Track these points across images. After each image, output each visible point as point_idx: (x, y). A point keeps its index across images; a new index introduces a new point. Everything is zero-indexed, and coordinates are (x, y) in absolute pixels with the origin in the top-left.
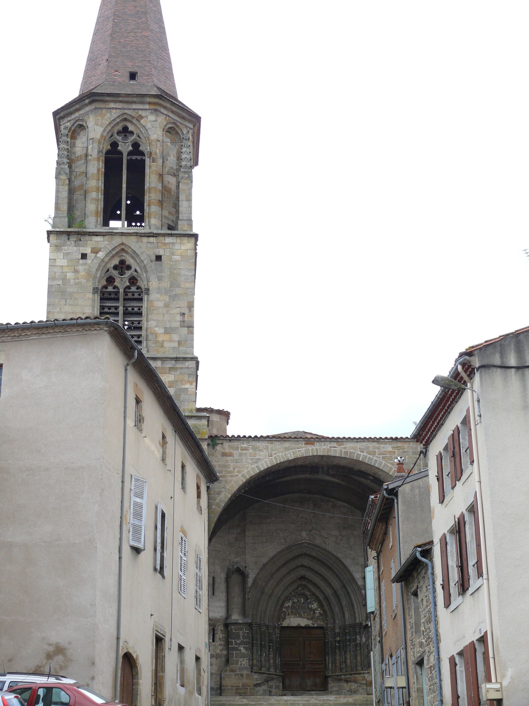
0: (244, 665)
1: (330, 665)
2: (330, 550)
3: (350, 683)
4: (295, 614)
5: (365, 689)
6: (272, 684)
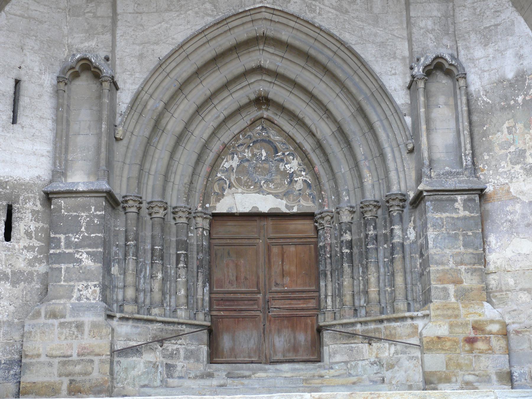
0: (87, 299)
1: (329, 299)
2: (325, 25)
3: (378, 344)
4: (247, 185)
5: (417, 358)
6: (175, 347)
